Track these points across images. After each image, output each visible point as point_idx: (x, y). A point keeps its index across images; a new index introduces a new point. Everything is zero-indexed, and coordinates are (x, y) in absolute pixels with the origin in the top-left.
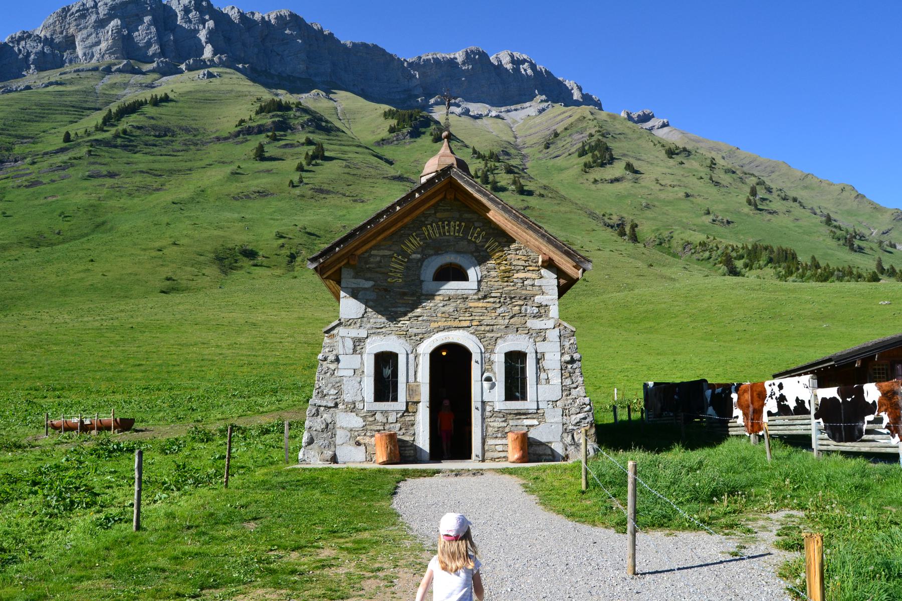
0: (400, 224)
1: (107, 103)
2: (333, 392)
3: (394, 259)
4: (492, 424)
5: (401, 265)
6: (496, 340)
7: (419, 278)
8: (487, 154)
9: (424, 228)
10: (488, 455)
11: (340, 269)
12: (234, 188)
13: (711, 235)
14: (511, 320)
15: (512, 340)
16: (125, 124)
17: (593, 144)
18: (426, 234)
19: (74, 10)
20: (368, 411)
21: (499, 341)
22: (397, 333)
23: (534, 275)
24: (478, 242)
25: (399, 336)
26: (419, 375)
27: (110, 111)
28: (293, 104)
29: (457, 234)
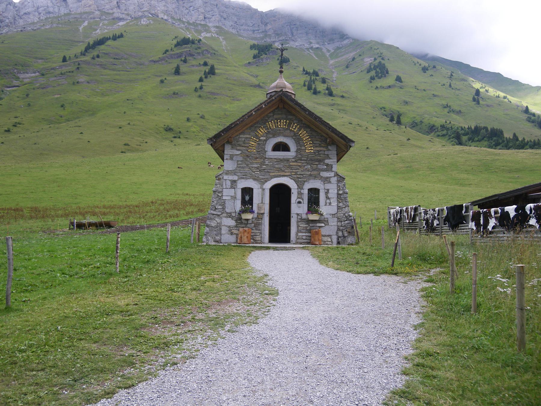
5: (255, 142)
8: (311, 71)
13: (448, 120)
17: (377, 65)
28: (196, 40)
29: (284, 127)
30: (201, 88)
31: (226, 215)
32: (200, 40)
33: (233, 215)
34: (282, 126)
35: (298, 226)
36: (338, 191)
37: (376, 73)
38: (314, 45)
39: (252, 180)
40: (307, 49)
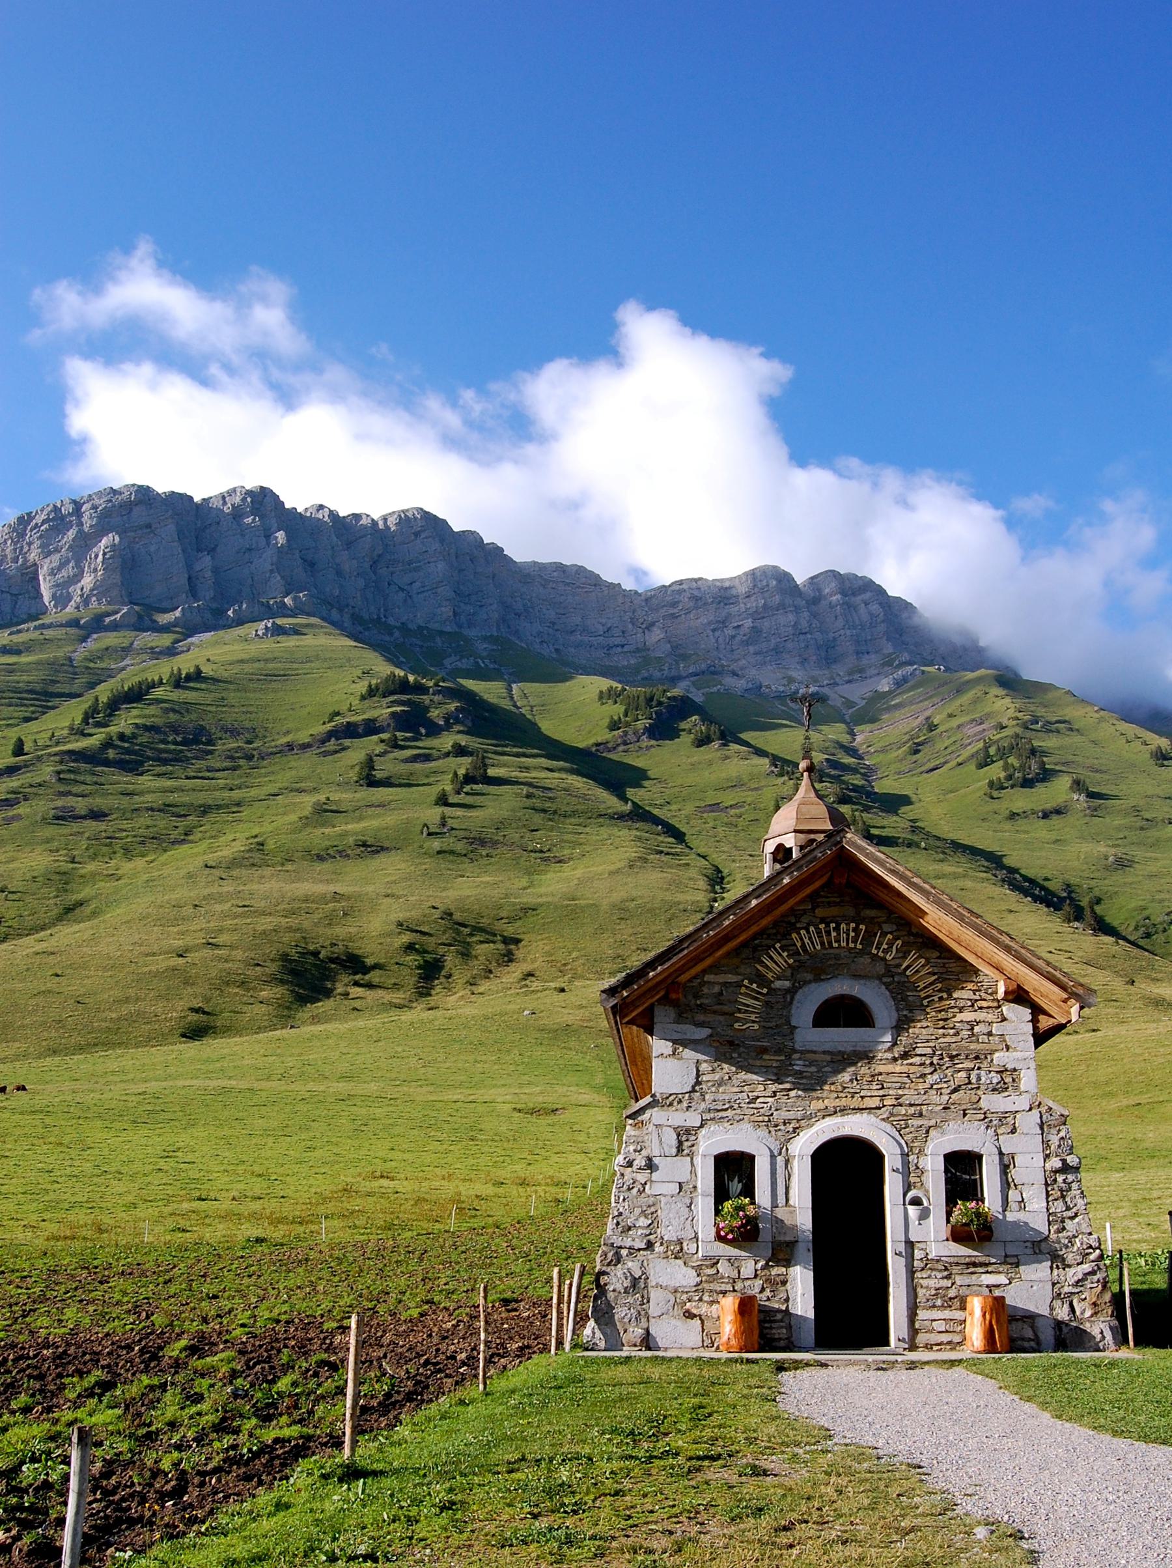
0: (754, 929)
1: (92, 685)
2: (644, 1222)
3: (743, 990)
4: (924, 1282)
5: (756, 999)
6: (927, 1132)
7: (788, 1023)
9: (794, 935)
10: (921, 1339)
11: (652, 1007)
12: (319, 836)
14: (953, 1096)
15: (956, 1132)
16: (126, 721)
18: (799, 944)
19: (39, 519)
20: (705, 1258)
21: (932, 1133)
22: (753, 1118)
23: (990, 1017)
24: (888, 957)
25: (757, 1125)
26: (794, 1192)
27: (97, 699)
29: (852, 945)
34: (844, 944)
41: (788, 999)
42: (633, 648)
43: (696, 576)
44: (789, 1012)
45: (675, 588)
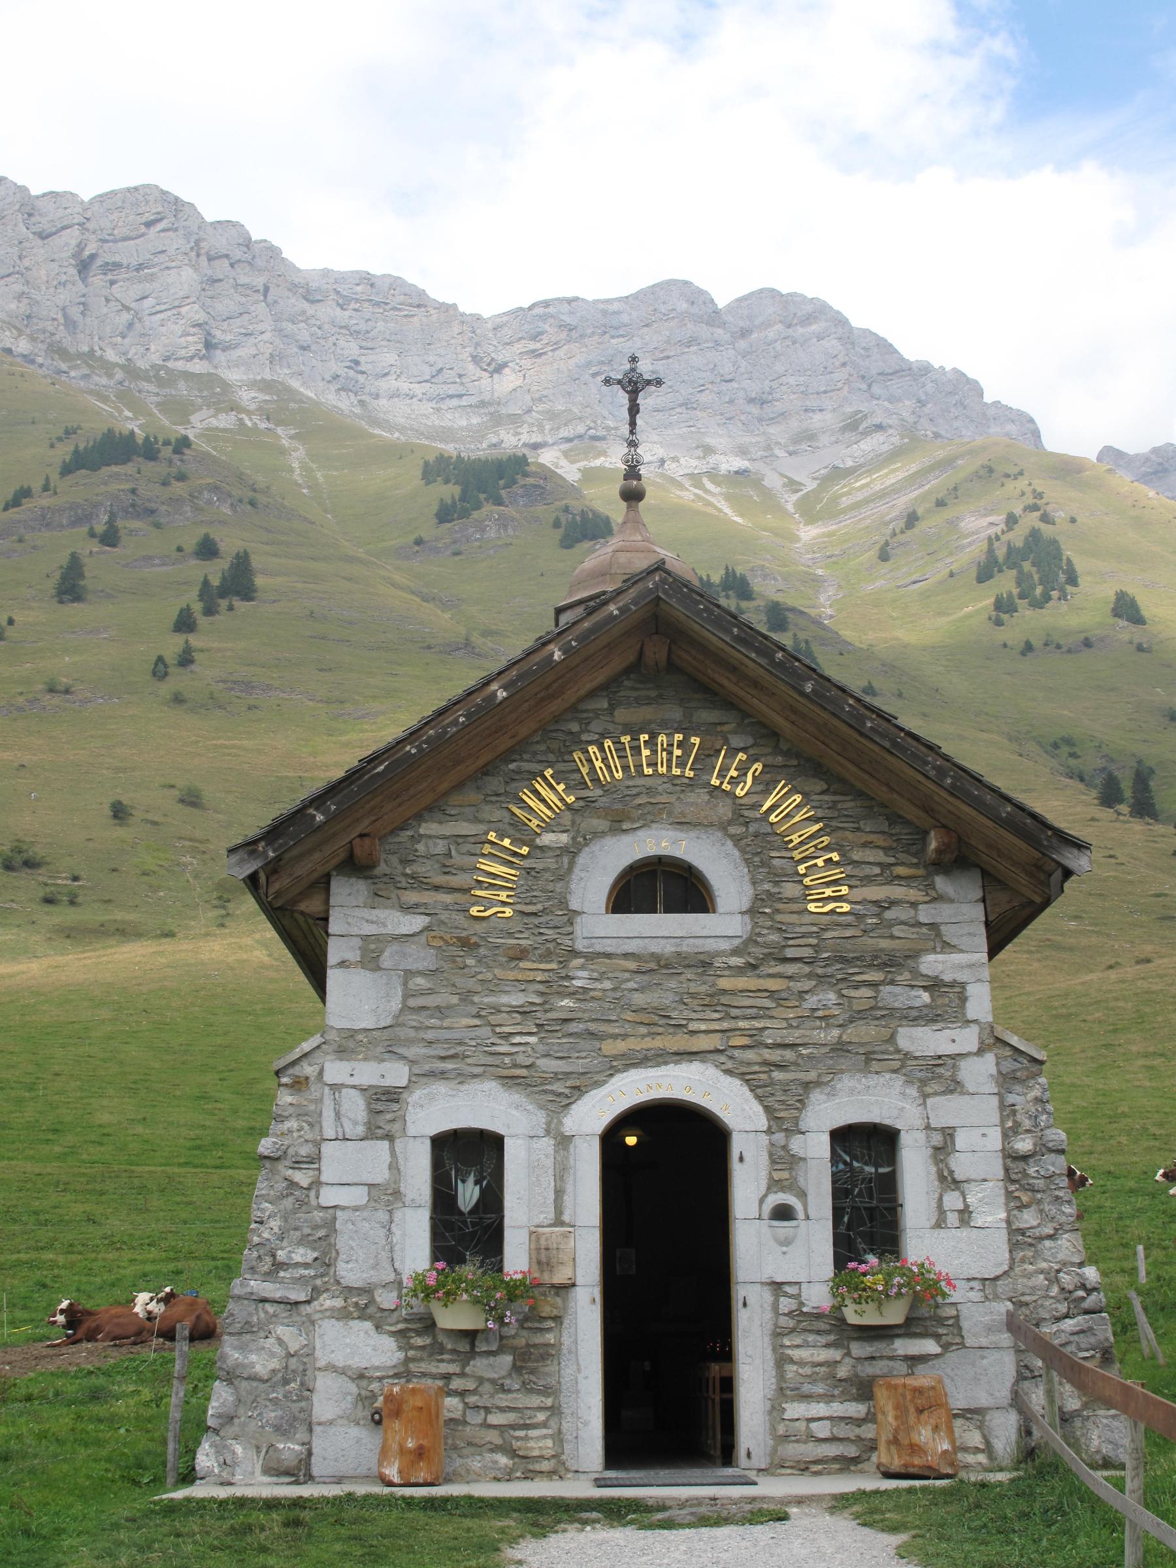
5: (510, 864)
7: (563, 903)
17: (1019, 544)
24: (739, 792)
28: (167, 443)
29: (676, 771)
30: (186, 659)
31: (339, 1303)
32: (183, 444)
33: (387, 1299)
34: (662, 770)
35: (782, 1361)
36: (1005, 1136)
37: (1019, 583)
38: (722, 458)
39: (492, 1085)
40: (691, 476)
41: (566, 866)
42: (473, 400)
43: (569, 294)
44: (568, 887)
45: (537, 311)
